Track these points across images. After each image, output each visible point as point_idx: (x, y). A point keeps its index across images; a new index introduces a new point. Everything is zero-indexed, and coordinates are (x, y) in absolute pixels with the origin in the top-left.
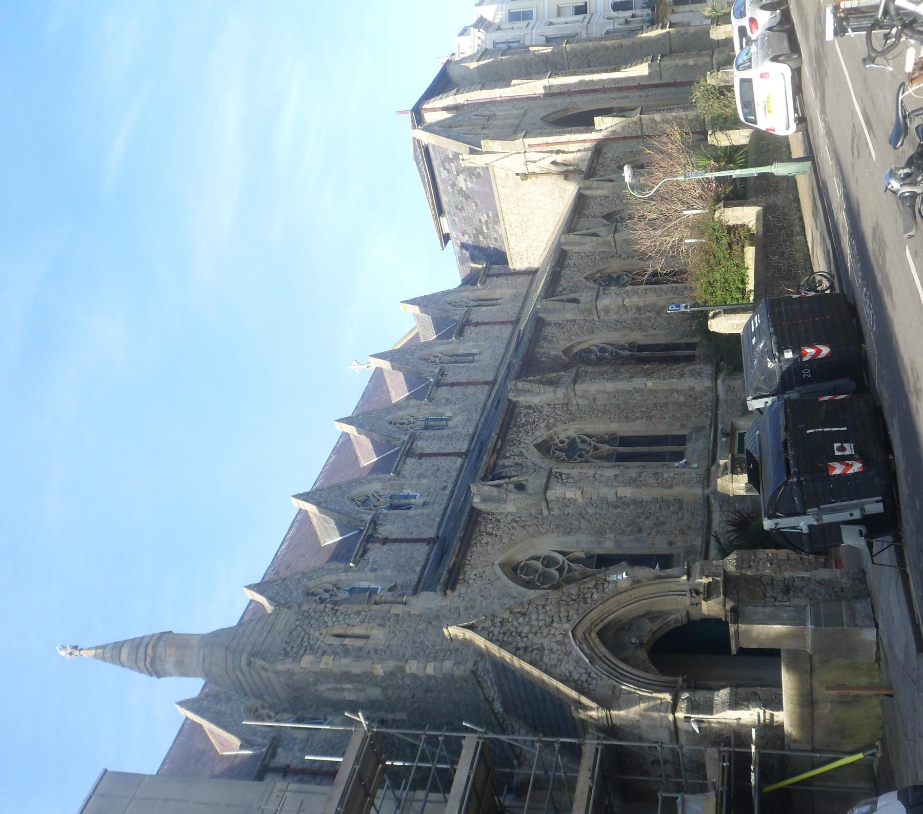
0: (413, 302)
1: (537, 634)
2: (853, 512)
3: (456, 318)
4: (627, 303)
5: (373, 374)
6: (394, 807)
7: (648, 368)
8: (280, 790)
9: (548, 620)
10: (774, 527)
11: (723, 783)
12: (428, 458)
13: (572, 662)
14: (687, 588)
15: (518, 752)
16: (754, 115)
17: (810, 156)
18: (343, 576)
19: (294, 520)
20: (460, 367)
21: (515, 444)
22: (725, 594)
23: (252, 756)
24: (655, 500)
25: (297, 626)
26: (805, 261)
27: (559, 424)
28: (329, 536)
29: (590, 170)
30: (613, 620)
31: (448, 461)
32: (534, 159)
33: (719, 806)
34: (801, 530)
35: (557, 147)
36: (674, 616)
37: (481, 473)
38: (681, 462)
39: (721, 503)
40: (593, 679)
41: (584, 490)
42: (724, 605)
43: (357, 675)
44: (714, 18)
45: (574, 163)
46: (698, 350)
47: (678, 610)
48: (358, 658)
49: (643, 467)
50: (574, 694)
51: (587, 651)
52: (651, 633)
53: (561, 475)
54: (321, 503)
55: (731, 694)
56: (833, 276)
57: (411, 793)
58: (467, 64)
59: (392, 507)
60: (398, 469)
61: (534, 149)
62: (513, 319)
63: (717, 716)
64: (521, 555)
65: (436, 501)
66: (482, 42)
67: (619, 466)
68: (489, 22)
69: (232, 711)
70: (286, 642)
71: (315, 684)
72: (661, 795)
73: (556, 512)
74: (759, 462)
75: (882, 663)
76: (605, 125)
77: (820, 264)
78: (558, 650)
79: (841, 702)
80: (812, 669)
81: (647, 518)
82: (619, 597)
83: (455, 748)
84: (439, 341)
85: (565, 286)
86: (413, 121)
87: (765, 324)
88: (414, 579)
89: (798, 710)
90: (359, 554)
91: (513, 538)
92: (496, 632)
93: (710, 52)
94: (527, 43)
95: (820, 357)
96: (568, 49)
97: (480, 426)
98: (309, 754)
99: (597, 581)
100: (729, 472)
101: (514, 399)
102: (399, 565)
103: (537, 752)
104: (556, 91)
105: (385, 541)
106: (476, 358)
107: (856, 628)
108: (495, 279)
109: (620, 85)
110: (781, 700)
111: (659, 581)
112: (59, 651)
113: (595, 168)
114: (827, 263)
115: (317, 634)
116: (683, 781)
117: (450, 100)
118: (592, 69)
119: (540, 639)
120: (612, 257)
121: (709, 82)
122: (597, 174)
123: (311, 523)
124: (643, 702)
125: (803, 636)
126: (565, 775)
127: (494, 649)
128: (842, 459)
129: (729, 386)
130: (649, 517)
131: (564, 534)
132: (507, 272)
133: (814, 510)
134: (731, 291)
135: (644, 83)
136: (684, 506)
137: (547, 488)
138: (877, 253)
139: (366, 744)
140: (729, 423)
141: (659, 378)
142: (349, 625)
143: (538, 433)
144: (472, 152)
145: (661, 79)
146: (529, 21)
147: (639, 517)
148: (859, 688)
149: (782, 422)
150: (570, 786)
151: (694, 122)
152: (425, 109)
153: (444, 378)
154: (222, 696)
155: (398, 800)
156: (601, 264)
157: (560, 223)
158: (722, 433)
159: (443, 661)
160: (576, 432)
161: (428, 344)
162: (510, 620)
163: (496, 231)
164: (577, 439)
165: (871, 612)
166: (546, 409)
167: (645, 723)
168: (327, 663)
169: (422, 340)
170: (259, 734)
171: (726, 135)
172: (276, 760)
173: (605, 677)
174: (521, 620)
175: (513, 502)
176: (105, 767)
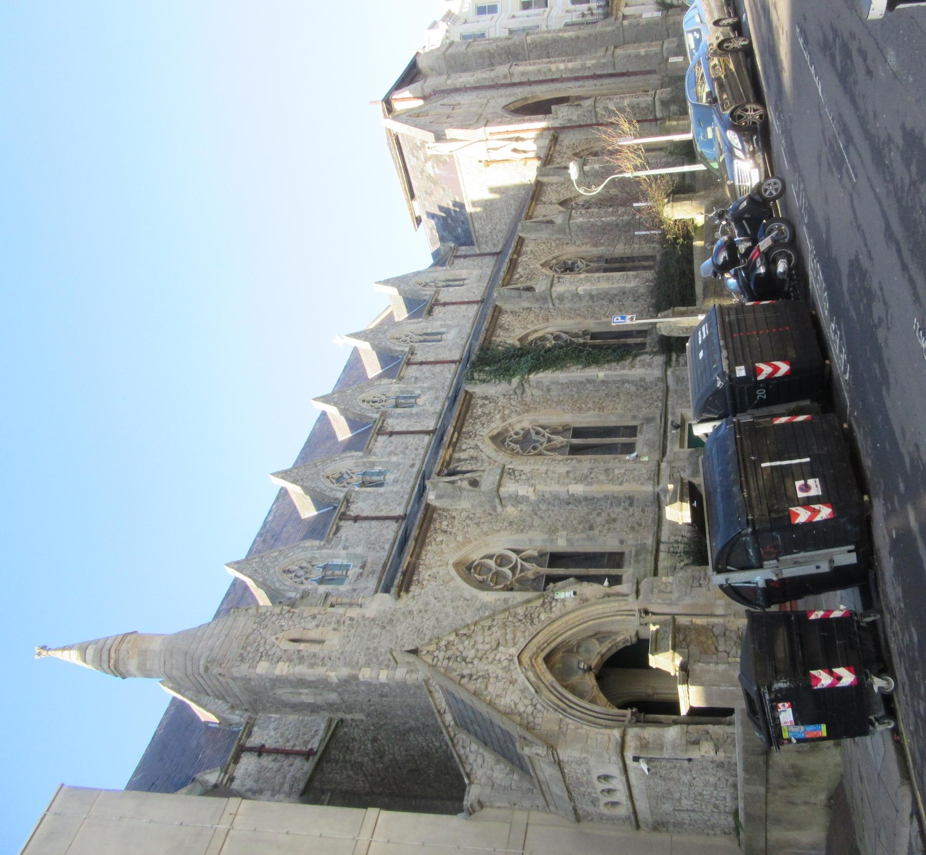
0: (387, 282)
1: (483, 660)
9: (494, 644)
13: (517, 692)
14: (637, 608)
20: (428, 346)
21: (470, 437)
27: (514, 415)
30: (562, 643)
32: (495, 147)
34: (757, 583)
35: (516, 135)
36: (622, 637)
40: (540, 711)
41: (537, 487)
43: (312, 682)
51: (533, 679)
52: (599, 657)
53: (514, 471)
59: (363, 484)
62: (479, 299)
67: (572, 459)
68: (456, 16)
71: (272, 689)
81: (599, 514)
85: (522, 273)
91: (467, 536)
92: (441, 657)
101: (470, 390)
105: (356, 519)
106: (444, 336)
108: (462, 260)
109: (577, 75)
111: (606, 599)
113: (551, 156)
115: (273, 638)
119: (485, 665)
128: (807, 503)
140: (679, 415)
143: (493, 425)
146: (494, 15)
151: (645, 110)
153: (413, 357)
156: (556, 251)
158: (672, 425)
160: (531, 423)
162: (456, 643)
164: (532, 431)
168: (282, 669)
172: (252, 739)
173: (551, 709)
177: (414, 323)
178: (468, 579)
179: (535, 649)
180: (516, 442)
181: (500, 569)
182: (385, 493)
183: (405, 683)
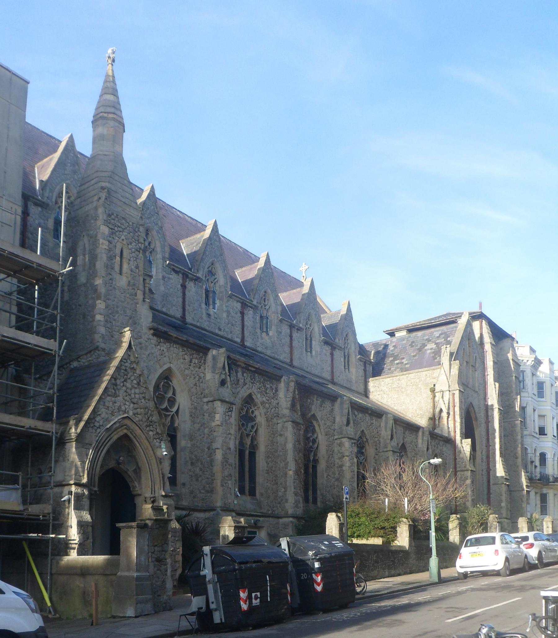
0: (349, 309)
2: (215, 603)
3: (337, 340)
4: (346, 459)
5: (298, 280)
6: (6, 291)
7: (301, 472)
8: (16, 210)
9: (135, 401)
10: (204, 553)
11: (29, 515)
12: (241, 318)
13: (107, 416)
14: (157, 495)
15: (45, 378)
16: (471, 546)
17: (442, 581)
18: (159, 256)
19: (197, 221)
20: (303, 342)
22: (156, 520)
23: (35, 189)
24: (213, 475)
25: (129, 223)
26: (372, 577)
27: (265, 410)
28: (187, 246)
29: (435, 435)
30: (135, 445)
31: (238, 332)
32: (444, 397)
33: (13, 512)
34: (203, 571)
35: (451, 413)
36: (137, 486)
37: (233, 356)
38: (238, 493)
39: (211, 519)
40: (96, 430)
42: (149, 519)
43: (94, 265)
44: (531, 520)
45: (440, 424)
46: (312, 505)
47: (141, 488)
48: (107, 267)
49: (235, 468)
50: (86, 417)
51: (115, 427)
53: (231, 411)
54: (211, 241)
55: (88, 522)
56: (364, 594)
57: (15, 303)
58: (511, 352)
59: (207, 291)
60: (233, 297)
61: (451, 397)
62: (335, 380)
63: (73, 512)
64: (177, 382)
65: (211, 323)
66: (525, 363)
67: (236, 451)
68: (538, 368)
69: (66, 174)
70: (117, 215)
71: (88, 235)
72: (20, 474)
73: (206, 407)
74: (247, 544)
75: (112, 620)
76: (465, 446)
77: (372, 586)
78: (115, 406)
79: (84, 593)
80: (106, 575)
81: (201, 469)
82: (150, 449)
83: (49, 334)
84: (321, 329)
85: (358, 416)
86: (474, 313)
87: (337, 550)
88: (158, 307)
89: (79, 565)
90: (175, 268)
92: (127, 364)
93: (509, 517)
94: (523, 394)
95: (315, 584)
96: (517, 422)
97: (262, 355)
98: (42, 231)
99: (161, 434)
100: (236, 524)
101: (282, 380)
102: (167, 296)
103: (46, 391)
104: (490, 414)
105: (184, 287)
106: (309, 353)
107: (135, 605)
108: (363, 368)
109: (491, 457)
110: (85, 555)
111: (161, 476)
112: (112, 48)
113: (436, 438)
114: (372, 591)
116: (29, 489)
117: (488, 339)
118: (503, 438)
120: (376, 449)
121: (491, 516)
122: (432, 440)
123: (196, 233)
124: (81, 464)
125: (129, 569)
126: (32, 410)
127: (115, 363)
128: (249, 597)
129: (288, 526)
130: (201, 471)
131: (191, 412)
132: (367, 376)
133: (216, 579)
134: (352, 529)
135: (491, 473)
136: (209, 494)
137: (222, 401)
138: (385, 623)
139: (50, 272)
141: (294, 479)
142: (129, 260)
143: (259, 396)
144: (451, 354)
145: (493, 484)
147: (201, 464)
148: (97, 605)
149: (274, 560)
150: (23, 413)
151: (463, 506)
152: (482, 322)
153: (296, 330)
154: (77, 167)
155: (10, 294)
157: (400, 414)
158: (257, 520)
159: (105, 326)
161: (319, 321)
162: (135, 374)
163: (395, 370)
164: (255, 423)
165: (145, 614)
166: (276, 402)
167: (67, 465)
168: (103, 244)
169: (322, 316)
170: (51, 194)
171: (456, 527)
172: (33, 207)
173: (97, 438)
174: (135, 382)
175: (213, 378)
176: (30, 83)
177: (319, 331)
178: (160, 378)
179: (132, 428)
180: (247, 412)
181: (167, 401)
182: (201, 308)
183: (95, 333)
